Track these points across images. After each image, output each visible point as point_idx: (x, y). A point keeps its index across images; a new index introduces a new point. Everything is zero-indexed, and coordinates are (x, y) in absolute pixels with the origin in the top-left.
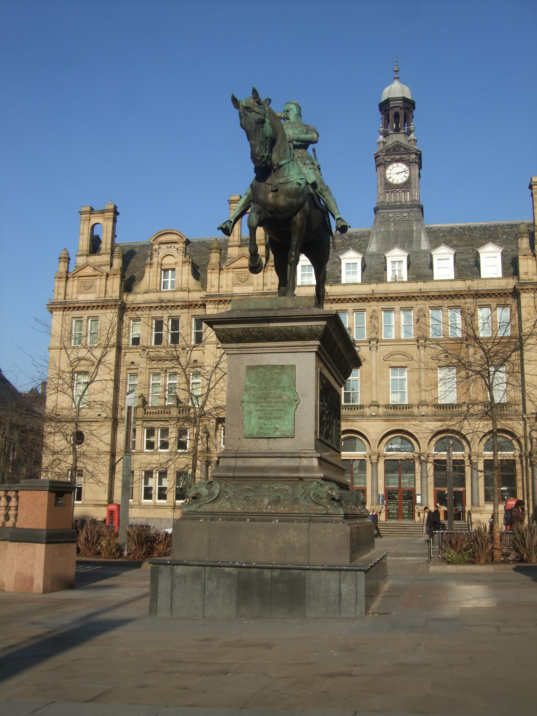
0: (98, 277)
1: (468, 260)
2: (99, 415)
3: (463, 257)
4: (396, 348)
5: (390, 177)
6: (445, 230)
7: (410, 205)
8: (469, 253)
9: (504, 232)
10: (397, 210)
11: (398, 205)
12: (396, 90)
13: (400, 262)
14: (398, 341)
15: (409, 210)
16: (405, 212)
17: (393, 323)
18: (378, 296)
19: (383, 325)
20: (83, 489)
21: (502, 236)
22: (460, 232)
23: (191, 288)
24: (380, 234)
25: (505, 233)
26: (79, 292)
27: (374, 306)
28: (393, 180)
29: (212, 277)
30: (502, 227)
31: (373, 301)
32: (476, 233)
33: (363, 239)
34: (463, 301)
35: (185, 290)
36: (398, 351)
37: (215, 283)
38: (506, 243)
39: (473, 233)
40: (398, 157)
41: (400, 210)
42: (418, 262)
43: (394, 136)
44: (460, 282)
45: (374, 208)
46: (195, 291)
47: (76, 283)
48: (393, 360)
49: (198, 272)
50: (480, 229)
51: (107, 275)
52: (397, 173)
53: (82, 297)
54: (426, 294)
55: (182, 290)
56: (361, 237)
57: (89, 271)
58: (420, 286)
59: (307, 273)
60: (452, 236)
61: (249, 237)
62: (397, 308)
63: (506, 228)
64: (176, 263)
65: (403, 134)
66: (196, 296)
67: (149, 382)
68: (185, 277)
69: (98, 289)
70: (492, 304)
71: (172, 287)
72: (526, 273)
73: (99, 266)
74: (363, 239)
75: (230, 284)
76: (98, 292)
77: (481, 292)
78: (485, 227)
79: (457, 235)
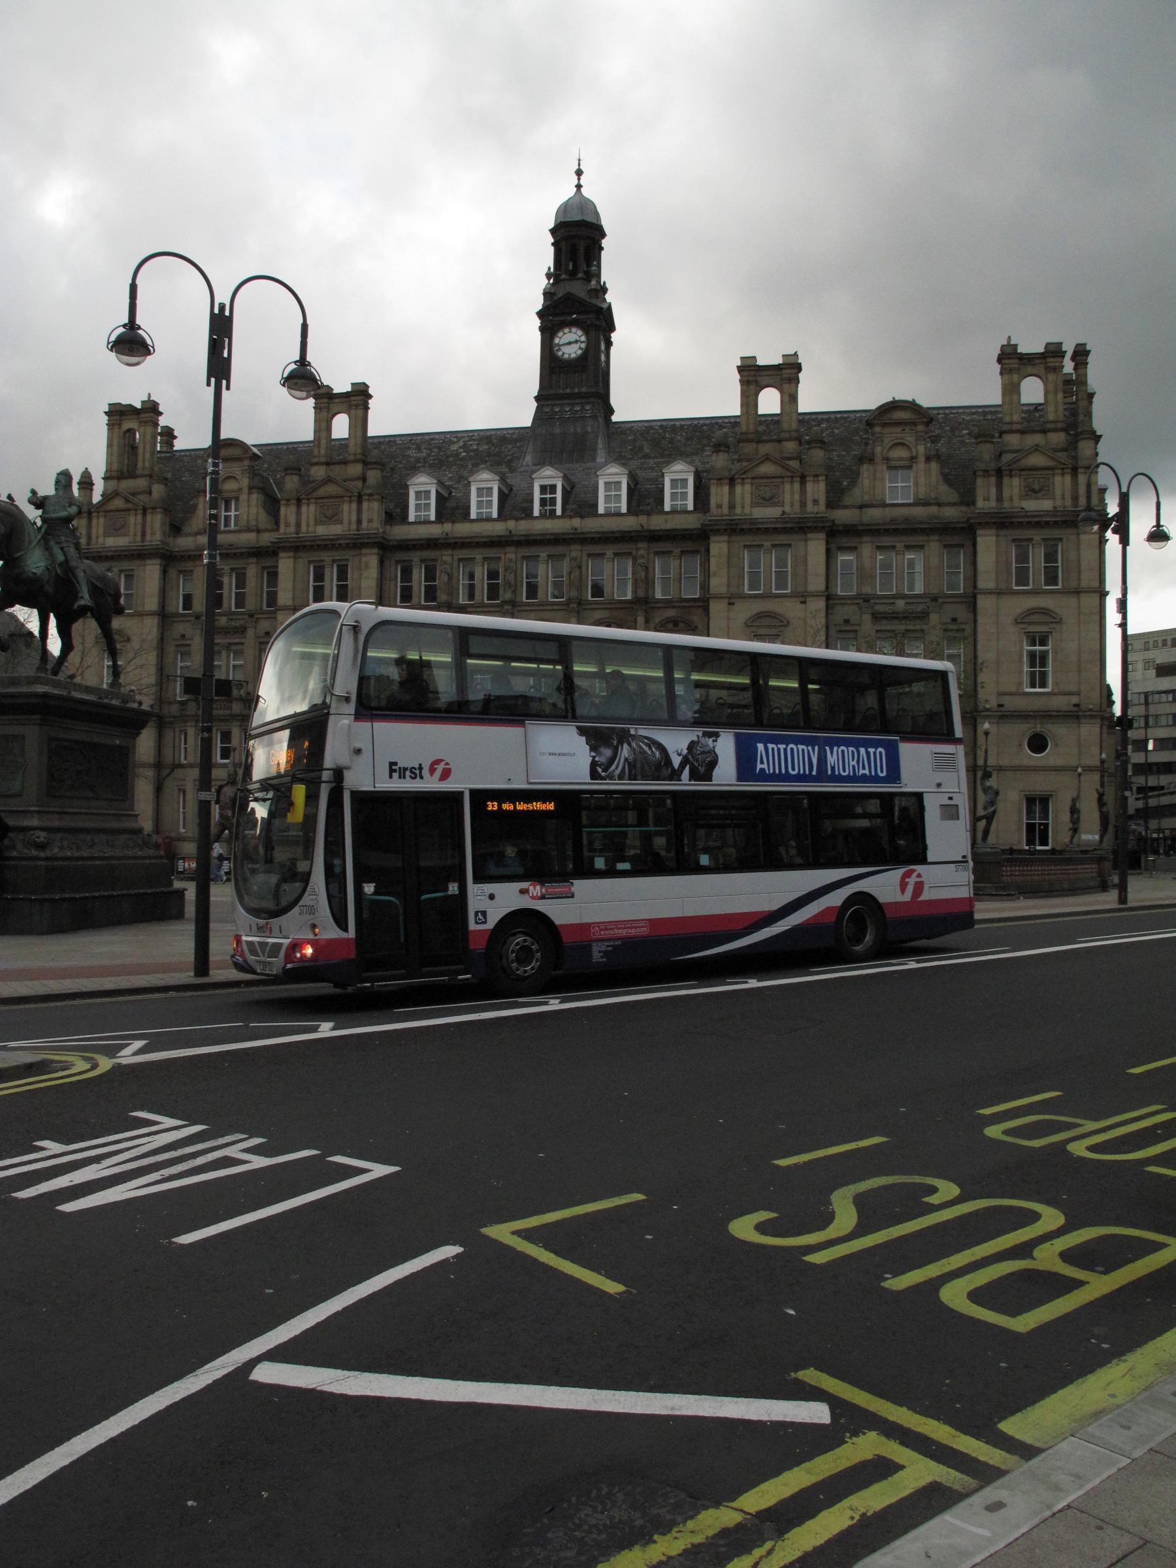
0: (1056, 471)
2: (1075, 705)
13: (553, 488)
23: (261, 526)
26: (107, 534)
27: (575, 551)
29: (287, 513)
31: (510, 545)
35: (252, 531)
37: (292, 519)
45: (1077, 345)
46: (267, 530)
47: (102, 520)
48: (1030, 623)
49: (272, 504)
51: (145, 510)
53: (321, 530)
55: (248, 530)
56: (516, 441)
57: (331, 489)
64: (240, 490)
66: (267, 538)
67: (1022, 648)
68: (253, 510)
69: (132, 528)
70: (898, 545)
71: (236, 525)
72: (720, 506)
73: (133, 494)
75: (312, 522)
76: (132, 533)
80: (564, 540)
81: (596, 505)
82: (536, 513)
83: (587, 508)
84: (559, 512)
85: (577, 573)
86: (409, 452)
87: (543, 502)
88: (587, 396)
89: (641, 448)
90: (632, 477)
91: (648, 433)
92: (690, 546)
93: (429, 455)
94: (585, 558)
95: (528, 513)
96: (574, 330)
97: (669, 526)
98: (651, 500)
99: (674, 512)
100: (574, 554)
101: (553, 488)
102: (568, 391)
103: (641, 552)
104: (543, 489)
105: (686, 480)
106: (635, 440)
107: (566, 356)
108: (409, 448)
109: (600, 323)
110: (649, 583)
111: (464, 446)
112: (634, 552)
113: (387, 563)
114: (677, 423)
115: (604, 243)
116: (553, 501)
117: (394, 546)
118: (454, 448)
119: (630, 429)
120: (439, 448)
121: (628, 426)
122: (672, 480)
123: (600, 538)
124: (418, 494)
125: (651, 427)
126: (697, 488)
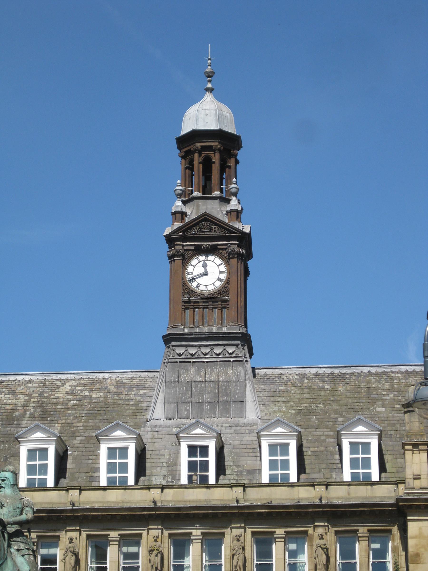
12: (205, 114)
33: (142, 392)
52: (209, 273)
74: (142, 392)
85: (241, 556)
87: (192, 466)
107: (202, 288)
111: (72, 392)
116: (205, 466)
122: (29, 450)
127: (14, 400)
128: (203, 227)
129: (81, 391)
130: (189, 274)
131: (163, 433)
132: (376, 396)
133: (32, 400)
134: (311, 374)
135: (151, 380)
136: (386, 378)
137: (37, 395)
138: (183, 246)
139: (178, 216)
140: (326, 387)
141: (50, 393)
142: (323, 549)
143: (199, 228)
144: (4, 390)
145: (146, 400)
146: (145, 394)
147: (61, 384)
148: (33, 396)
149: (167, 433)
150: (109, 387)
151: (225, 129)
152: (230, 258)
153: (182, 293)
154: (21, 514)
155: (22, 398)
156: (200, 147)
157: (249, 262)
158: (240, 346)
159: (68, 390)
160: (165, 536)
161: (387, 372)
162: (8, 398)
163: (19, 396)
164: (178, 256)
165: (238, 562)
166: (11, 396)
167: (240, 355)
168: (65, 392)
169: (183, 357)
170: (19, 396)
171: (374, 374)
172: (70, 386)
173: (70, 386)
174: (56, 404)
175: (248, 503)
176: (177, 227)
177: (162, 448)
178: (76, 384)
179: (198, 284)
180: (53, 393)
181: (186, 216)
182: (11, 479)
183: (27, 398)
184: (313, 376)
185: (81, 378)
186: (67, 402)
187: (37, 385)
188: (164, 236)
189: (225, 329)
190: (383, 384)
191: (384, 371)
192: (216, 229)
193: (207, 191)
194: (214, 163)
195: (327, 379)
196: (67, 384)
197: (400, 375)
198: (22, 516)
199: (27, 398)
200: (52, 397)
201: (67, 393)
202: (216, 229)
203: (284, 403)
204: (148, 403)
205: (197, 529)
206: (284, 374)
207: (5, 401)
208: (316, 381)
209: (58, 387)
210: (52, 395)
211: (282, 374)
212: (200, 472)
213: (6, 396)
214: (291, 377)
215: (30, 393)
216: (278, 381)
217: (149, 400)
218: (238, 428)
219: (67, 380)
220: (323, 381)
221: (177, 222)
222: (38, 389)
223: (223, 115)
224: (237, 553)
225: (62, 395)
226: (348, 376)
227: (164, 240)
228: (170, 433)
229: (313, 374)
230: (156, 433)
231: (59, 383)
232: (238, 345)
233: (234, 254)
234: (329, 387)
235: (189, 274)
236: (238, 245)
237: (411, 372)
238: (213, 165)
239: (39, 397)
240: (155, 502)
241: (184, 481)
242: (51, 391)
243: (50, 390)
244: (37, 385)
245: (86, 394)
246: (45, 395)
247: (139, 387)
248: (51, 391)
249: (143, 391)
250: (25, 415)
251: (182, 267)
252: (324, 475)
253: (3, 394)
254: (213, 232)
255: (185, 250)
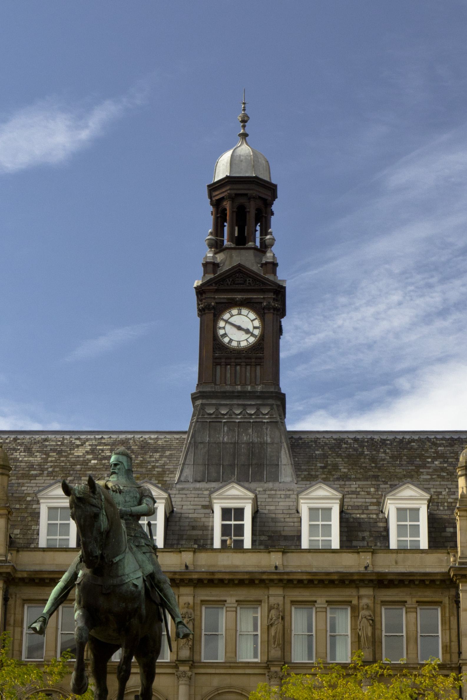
1: (367, 508)
3: (359, 501)
4: (228, 681)
5: (225, 335)
6: (326, 444)
7: (262, 392)
8: (369, 493)
9: (436, 452)
10: (235, 402)
11: (238, 392)
13: (239, 513)
14: (230, 667)
15: (259, 402)
16: (251, 405)
17: (222, 630)
18: (195, 576)
19: (203, 633)
20: (221, 520)
21: (432, 462)
22: (355, 450)
24: (201, 446)
25: (438, 456)
28: (231, 340)
30: (434, 444)
32: (385, 452)
33: (168, 453)
34: (354, 592)
36: (230, 687)
38: (439, 476)
39: (378, 451)
40: (239, 297)
41: (240, 402)
42: (272, 508)
43: (234, 253)
44: (350, 555)
50: (391, 444)
54: (285, 577)
58: (273, 560)
59: (59, 522)
60: (339, 456)
61: (333, 548)
62: (231, 600)
63: (440, 445)
65: (251, 252)
74: (168, 453)
77: (389, 577)
78: (401, 441)
79: (349, 456)
80: (262, 581)
81: (386, 538)
82: (217, 544)
83: (289, 541)
84: (248, 544)
85: (280, 626)
86: (16, 454)
87: (226, 530)
88: (262, 396)
89: (335, 467)
90: (255, 501)
91: (340, 447)
92: (429, 595)
93: (45, 461)
94: (288, 605)
95: (203, 543)
96: (245, 311)
97: (401, 569)
98: (367, 534)
99: (49, 549)
100: (272, 600)
101: (239, 513)
102: (239, 388)
103: (365, 601)
104: (226, 513)
105: (418, 510)
106: (325, 456)
107: (234, 344)
108: (16, 450)
109: (270, 300)
110: (284, 642)
111: (93, 451)
112: (355, 602)
113: (11, 602)
114: (376, 437)
115: (276, 200)
116: (240, 530)
117: (22, 580)
118: (79, 452)
119: (316, 441)
120: (60, 453)
121: (313, 436)
122: (50, 508)
123: (311, 581)
124: (226, 513)
125: (342, 440)
126: (432, 520)
127: (31, 459)
128: (237, 279)
129: (103, 450)
130: (220, 328)
131: (193, 496)
132: (421, 463)
133: (50, 459)
134: (349, 438)
135: (178, 441)
136: (430, 444)
137: (55, 454)
138: (214, 298)
139: (210, 267)
140: (366, 453)
141: (69, 452)
142: (368, 620)
143: (233, 280)
144: (19, 447)
145: (173, 462)
146: (171, 455)
147: (80, 443)
148: (50, 454)
149: (196, 496)
150: (132, 447)
151: (261, 177)
152: (265, 313)
153: (213, 348)
154: (140, 503)
155: (38, 456)
156: (234, 195)
157: (282, 320)
158: (275, 406)
159: (88, 450)
160: (197, 603)
161: (431, 439)
162: (23, 457)
163: (35, 454)
164: (209, 309)
165: (276, 633)
166: (26, 454)
167: (274, 416)
168: (84, 452)
169: (213, 416)
170: (35, 454)
171: (417, 440)
172: (90, 445)
173: (90, 445)
174: (74, 464)
175: (288, 570)
176: (208, 279)
177: (191, 511)
178: (96, 443)
179: (231, 339)
180: (72, 452)
181: (219, 267)
182: (125, 464)
183: (44, 456)
184: (352, 441)
185: (102, 438)
186: (87, 461)
187: (55, 443)
188: (195, 288)
189: (259, 388)
190: (427, 451)
191: (427, 437)
192: (251, 282)
193: (241, 241)
194: (249, 212)
195: (366, 444)
196: (87, 443)
197: (444, 442)
198: (140, 507)
199: (44, 456)
200: (70, 456)
201: (87, 452)
202: (251, 282)
203: (322, 468)
204: (175, 464)
205: (231, 595)
206: (320, 439)
207: (20, 459)
208: (355, 446)
209: (78, 446)
210: (70, 454)
211: (317, 438)
212: (234, 536)
213: (21, 454)
214: (327, 442)
215: (47, 452)
216: (314, 446)
217: (176, 462)
218: (273, 492)
219: (87, 440)
220: (362, 446)
221: (209, 274)
222: (56, 447)
223: (259, 162)
224: (276, 623)
225: (81, 454)
226: (389, 442)
227: (194, 292)
228: (200, 496)
229: (352, 439)
230: (184, 496)
231: (78, 442)
232: (271, 405)
233: (269, 309)
234: (368, 453)
235: (220, 328)
236: (274, 299)
237: (456, 440)
238: (247, 214)
239: (57, 456)
240: (187, 567)
241: (217, 544)
242: (70, 450)
243: (68, 449)
244: (55, 443)
245: (107, 454)
246: (64, 454)
247: (163, 449)
248: (70, 450)
249: (169, 452)
250: (43, 474)
251: (214, 321)
252: (368, 544)
253: (19, 451)
254: (248, 284)
255: (216, 303)
